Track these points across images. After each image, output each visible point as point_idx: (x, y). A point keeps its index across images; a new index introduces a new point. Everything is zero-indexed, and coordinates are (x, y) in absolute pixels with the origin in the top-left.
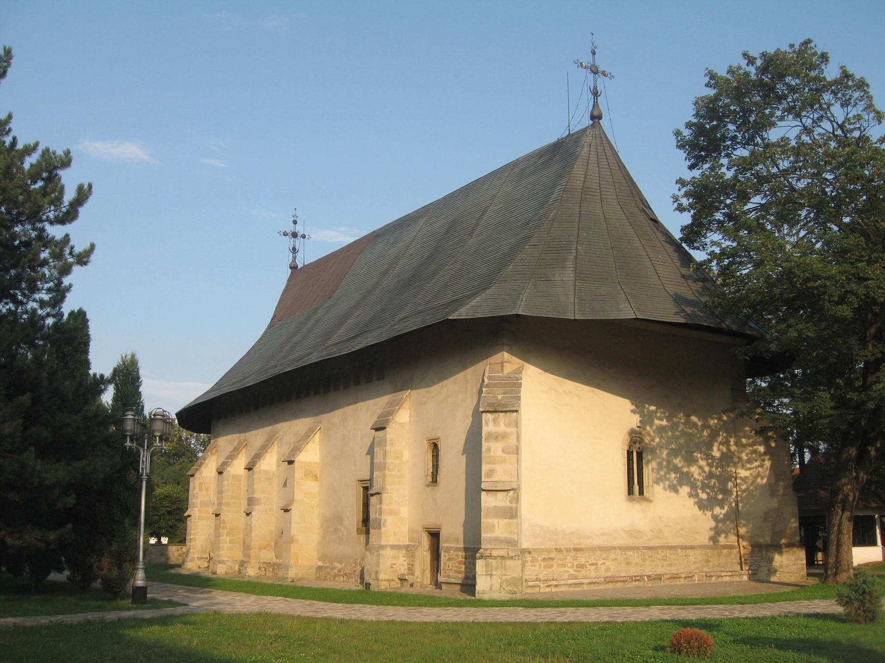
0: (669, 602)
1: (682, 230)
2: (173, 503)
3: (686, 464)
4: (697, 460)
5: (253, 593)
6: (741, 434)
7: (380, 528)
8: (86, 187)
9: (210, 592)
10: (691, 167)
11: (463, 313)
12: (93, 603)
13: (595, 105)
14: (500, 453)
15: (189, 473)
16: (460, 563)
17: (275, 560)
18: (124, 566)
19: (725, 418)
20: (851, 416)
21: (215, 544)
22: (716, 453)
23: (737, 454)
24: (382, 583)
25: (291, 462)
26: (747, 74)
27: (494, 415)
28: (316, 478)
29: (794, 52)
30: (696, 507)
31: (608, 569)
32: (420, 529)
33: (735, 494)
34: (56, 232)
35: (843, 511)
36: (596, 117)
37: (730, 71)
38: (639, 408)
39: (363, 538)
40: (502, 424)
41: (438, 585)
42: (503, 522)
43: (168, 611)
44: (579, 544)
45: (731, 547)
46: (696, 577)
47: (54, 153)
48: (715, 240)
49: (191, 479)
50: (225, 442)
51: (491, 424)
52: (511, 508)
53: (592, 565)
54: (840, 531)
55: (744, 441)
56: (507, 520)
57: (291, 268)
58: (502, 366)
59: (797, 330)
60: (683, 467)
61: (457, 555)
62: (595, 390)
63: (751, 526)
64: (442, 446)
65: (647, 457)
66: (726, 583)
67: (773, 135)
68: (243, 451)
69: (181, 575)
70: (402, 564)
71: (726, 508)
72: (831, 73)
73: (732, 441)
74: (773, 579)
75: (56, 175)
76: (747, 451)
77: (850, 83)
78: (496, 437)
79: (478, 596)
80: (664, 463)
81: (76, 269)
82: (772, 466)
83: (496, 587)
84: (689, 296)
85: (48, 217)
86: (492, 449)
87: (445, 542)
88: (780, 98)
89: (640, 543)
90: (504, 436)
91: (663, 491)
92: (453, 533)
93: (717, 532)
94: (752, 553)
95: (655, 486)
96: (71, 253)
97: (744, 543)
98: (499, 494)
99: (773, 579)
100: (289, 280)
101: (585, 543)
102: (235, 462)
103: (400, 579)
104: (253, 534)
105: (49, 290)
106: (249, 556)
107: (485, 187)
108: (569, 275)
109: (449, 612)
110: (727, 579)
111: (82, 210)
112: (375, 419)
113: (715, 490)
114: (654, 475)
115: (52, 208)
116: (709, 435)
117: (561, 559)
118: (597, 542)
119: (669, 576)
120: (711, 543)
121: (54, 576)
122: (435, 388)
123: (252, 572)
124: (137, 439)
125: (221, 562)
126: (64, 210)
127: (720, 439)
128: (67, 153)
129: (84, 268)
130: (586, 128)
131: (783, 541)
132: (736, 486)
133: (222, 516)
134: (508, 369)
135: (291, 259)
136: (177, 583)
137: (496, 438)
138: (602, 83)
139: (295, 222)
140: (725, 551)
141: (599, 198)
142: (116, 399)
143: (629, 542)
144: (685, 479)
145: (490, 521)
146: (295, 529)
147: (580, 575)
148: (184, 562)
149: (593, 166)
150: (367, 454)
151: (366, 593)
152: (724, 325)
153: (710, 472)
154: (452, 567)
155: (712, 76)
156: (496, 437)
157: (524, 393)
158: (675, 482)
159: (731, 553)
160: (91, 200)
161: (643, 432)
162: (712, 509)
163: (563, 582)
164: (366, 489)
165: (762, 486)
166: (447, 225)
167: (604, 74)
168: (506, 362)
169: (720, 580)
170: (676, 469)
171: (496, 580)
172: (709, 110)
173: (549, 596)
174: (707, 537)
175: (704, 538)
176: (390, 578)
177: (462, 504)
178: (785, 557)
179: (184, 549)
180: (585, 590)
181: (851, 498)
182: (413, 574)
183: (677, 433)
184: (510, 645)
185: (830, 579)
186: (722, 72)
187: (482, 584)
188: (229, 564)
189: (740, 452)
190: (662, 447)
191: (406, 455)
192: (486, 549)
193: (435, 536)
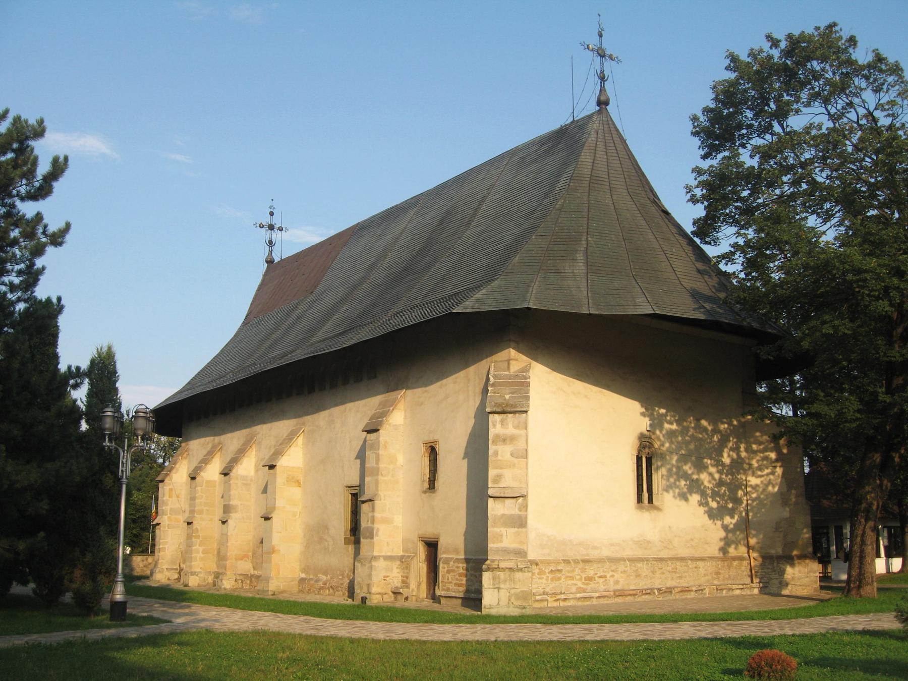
0: (696, 617)
1: (694, 224)
2: (138, 510)
3: (696, 471)
4: (707, 467)
5: (237, 607)
6: (752, 440)
7: (372, 538)
8: (62, 159)
9: (189, 607)
10: (704, 157)
11: (468, 306)
13: (602, 90)
14: (508, 456)
15: (159, 478)
16: (460, 575)
17: (252, 572)
18: (99, 579)
19: (735, 423)
20: (877, 421)
21: (186, 554)
22: (726, 460)
23: (747, 461)
24: (374, 597)
26: (771, 57)
28: (299, 484)
29: (820, 35)
30: (706, 516)
31: (617, 582)
32: (416, 539)
33: (745, 502)
34: (28, 209)
35: (866, 521)
36: (603, 103)
37: (752, 54)
38: (649, 411)
39: (351, 548)
40: (510, 426)
41: (435, 598)
43: (151, 629)
44: (588, 555)
45: (741, 559)
46: (707, 591)
47: (26, 121)
48: (727, 237)
49: (161, 485)
50: (197, 446)
51: (498, 426)
52: (520, 517)
53: (600, 577)
54: (863, 543)
55: (754, 447)
56: (516, 529)
57: (267, 262)
58: (509, 364)
59: (834, 327)
60: (693, 473)
61: (458, 567)
62: (604, 391)
63: (761, 536)
65: (656, 463)
66: (738, 596)
67: (796, 123)
68: (218, 455)
69: (150, 588)
70: (395, 576)
71: (736, 517)
72: (861, 55)
73: (742, 446)
75: (28, 146)
76: (758, 458)
77: (883, 67)
78: (504, 440)
79: (484, 611)
80: (674, 470)
81: (50, 250)
82: (784, 474)
83: (504, 601)
85: (18, 192)
86: (499, 452)
87: (444, 553)
88: (803, 84)
89: (651, 553)
90: (511, 439)
91: (673, 499)
92: (453, 542)
93: (727, 543)
94: (762, 565)
95: (665, 494)
96: (44, 233)
97: (754, 555)
98: (508, 501)
100: (265, 275)
101: (594, 554)
102: (209, 466)
103: (394, 593)
104: (229, 544)
105: (20, 273)
107: (481, 176)
108: (580, 267)
109: (463, 629)
110: (738, 592)
111: (56, 185)
113: (725, 498)
114: (664, 482)
115: (24, 182)
116: (719, 441)
117: (569, 572)
118: (606, 553)
119: (679, 589)
120: (721, 554)
121: (17, 589)
122: (433, 388)
123: (227, 584)
124: (116, 439)
125: (193, 573)
126: (37, 184)
127: (730, 444)
128: (41, 122)
129: (59, 249)
130: (592, 114)
131: (795, 553)
132: (746, 494)
133: (196, 525)
134: (515, 367)
135: (267, 253)
136: (150, 597)
139: (272, 214)
140: (735, 563)
142: (90, 395)
143: (639, 553)
144: (695, 486)
145: (497, 530)
146: (276, 539)
147: (589, 588)
148: (152, 573)
149: (600, 154)
151: (362, 610)
152: (745, 323)
153: (720, 479)
154: (452, 580)
155: (734, 59)
156: (504, 440)
157: (533, 393)
158: (685, 490)
159: (741, 565)
160: (67, 174)
161: (653, 437)
163: (572, 596)
164: (355, 496)
166: (442, 214)
167: (611, 57)
168: (512, 360)
169: (731, 593)
170: (686, 476)
172: (728, 95)
173: (559, 611)
174: (717, 548)
175: (714, 550)
176: (383, 591)
178: (797, 569)
180: (595, 605)
181: (874, 507)
182: (408, 587)
183: (687, 438)
184: (558, 668)
185: (853, 592)
186: (744, 57)
187: (489, 598)
188: (202, 575)
189: (751, 459)
190: (671, 453)
191: (401, 459)
192: (493, 561)
193: (432, 546)
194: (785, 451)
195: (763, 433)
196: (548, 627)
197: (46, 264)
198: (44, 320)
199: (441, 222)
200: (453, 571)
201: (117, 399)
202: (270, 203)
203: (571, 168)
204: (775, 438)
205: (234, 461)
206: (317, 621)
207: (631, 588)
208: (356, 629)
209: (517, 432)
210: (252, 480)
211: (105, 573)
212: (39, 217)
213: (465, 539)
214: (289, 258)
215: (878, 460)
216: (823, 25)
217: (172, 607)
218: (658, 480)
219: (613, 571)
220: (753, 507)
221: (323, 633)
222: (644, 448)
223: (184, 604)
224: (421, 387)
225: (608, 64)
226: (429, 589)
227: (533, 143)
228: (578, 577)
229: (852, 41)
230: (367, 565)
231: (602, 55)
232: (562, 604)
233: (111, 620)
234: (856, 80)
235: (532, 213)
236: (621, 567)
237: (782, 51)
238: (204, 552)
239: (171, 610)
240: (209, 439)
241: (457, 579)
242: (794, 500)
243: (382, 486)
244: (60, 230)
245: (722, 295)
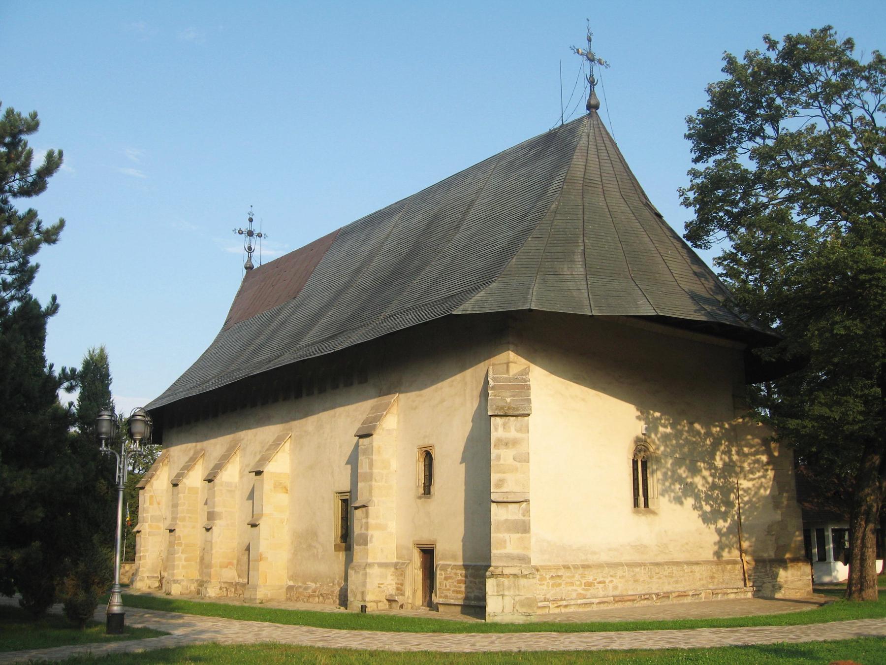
0: (713, 624)
1: (686, 227)
3: (690, 474)
4: (701, 471)
6: (743, 443)
7: (366, 544)
8: (56, 154)
9: (180, 617)
10: (696, 161)
11: (467, 307)
12: (56, 633)
13: (592, 94)
14: (510, 461)
15: (139, 485)
16: (459, 582)
17: (237, 579)
19: (727, 426)
21: (168, 561)
22: (719, 463)
23: (739, 464)
25: (259, 473)
26: (767, 59)
27: (504, 419)
28: (286, 490)
32: (411, 545)
33: (737, 506)
34: (20, 205)
35: (867, 523)
36: (592, 107)
37: (749, 57)
39: (342, 555)
40: (513, 429)
41: (431, 605)
42: (516, 536)
45: (734, 562)
46: (703, 595)
47: (19, 115)
50: (178, 453)
51: (500, 429)
52: (524, 522)
53: (600, 583)
54: (864, 545)
55: (746, 450)
56: (520, 535)
57: (246, 268)
58: (508, 367)
59: (845, 328)
60: (687, 477)
61: (456, 574)
63: (754, 539)
64: (437, 455)
65: (652, 466)
66: (734, 601)
67: (790, 125)
68: (201, 461)
70: (390, 584)
71: (729, 520)
72: (862, 56)
73: (734, 450)
74: (778, 595)
75: (20, 141)
76: (749, 461)
79: (489, 620)
80: (669, 473)
81: (44, 247)
82: (775, 476)
83: (509, 608)
84: (703, 292)
86: (500, 456)
87: (441, 559)
89: (648, 558)
93: (721, 546)
94: (755, 569)
95: (661, 498)
96: (38, 229)
97: (747, 558)
98: (511, 506)
99: (778, 595)
101: (592, 559)
102: (191, 473)
103: (389, 600)
104: (214, 551)
105: (12, 271)
106: (209, 575)
110: (732, 596)
111: (50, 181)
113: (719, 502)
114: (660, 486)
115: (18, 176)
116: (712, 444)
117: (569, 577)
118: (604, 558)
119: (677, 594)
120: (716, 558)
123: (212, 592)
125: (176, 582)
126: (30, 179)
127: (722, 448)
129: (53, 246)
131: (788, 556)
133: (178, 532)
134: (514, 370)
137: (506, 444)
139: (251, 220)
140: (729, 567)
141: (601, 190)
143: (637, 558)
144: (689, 490)
145: (501, 535)
147: (589, 594)
148: (132, 582)
149: (592, 157)
150: (347, 463)
151: (363, 620)
153: (713, 482)
154: (451, 586)
156: (507, 444)
158: (680, 494)
159: (734, 569)
161: (648, 440)
162: (715, 522)
163: (573, 602)
164: (345, 502)
165: (766, 498)
166: (430, 218)
168: (511, 363)
169: (726, 597)
170: (680, 480)
171: (508, 602)
172: (723, 99)
174: (712, 552)
175: (708, 554)
176: (377, 599)
177: (461, 518)
179: (134, 566)
180: (595, 612)
181: (874, 510)
182: (403, 595)
183: (681, 441)
185: (856, 595)
187: (493, 605)
190: (666, 456)
191: (394, 465)
192: (497, 567)
193: (428, 553)
194: (776, 454)
195: (754, 436)
196: (566, 635)
197: (41, 263)
198: (32, 322)
199: (429, 226)
200: (450, 578)
201: (109, 403)
202: (249, 210)
203: (564, 171)
204: (766, 442)
205: (218, 467)
206: (320, 631)
207: (630, 593)
208: (366, 640)
209: (519, 435)
210: (236, 487)
211: (99, 583)
212: (32, 214)
213: (464, 545)
214: (269, 263)
215: (877, 462)
216: (819, 27)
217: (163, 616)
218: (654, 483)
219: (611, 576)
220: (745, 511)
222: (640, 451)
223: (174, 614)
224: (415, 390)
225: (597, 68)
226: (424, 597)
227: (521, 147)
228: (578, 583)
229: (849, 43)
230: (361, 573)
231: (592, 60)
232: (563, 610)
233: (108, 632)
234: (857, 82)
235: (526, 215)
236: (620, 573)
237: (779, 52)
238: (186, 560)
239: (164, 621)
240: (191, 445)
241: (455, 586)
242: (785, 503)
243: (375, 492)
244: (54, 227)
245: (720, 298)
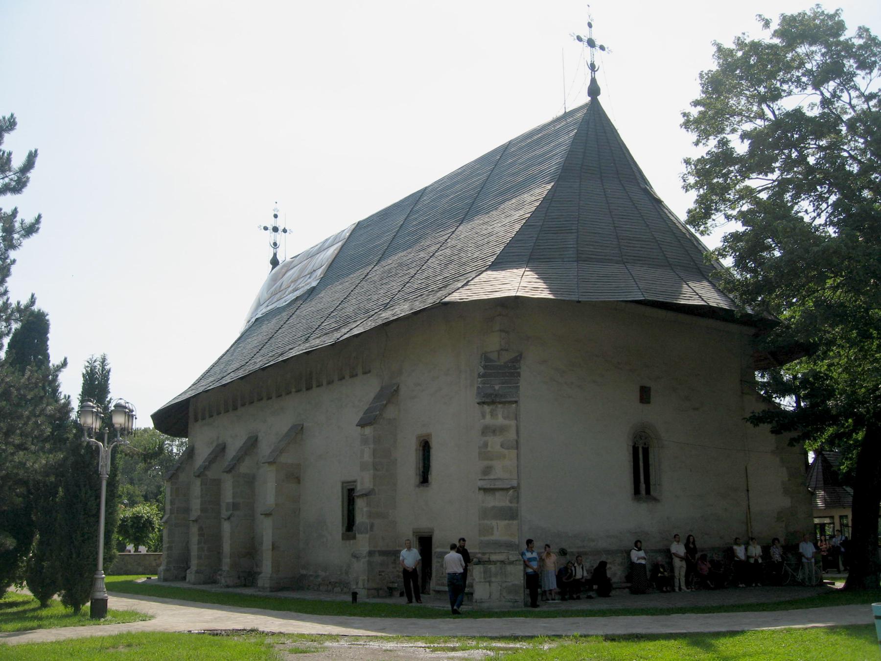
13: (593, 81)
36: (594, 90)
40: (500, 416)
42: (503, 523)
52: (511, 509)
56: (507, 522)
98: (498, 494)
112: (361, 415)
138: (599, 57)
139: (276, 216)
167: (602, 48)
209: (507, 422)
221: (62, 638)
